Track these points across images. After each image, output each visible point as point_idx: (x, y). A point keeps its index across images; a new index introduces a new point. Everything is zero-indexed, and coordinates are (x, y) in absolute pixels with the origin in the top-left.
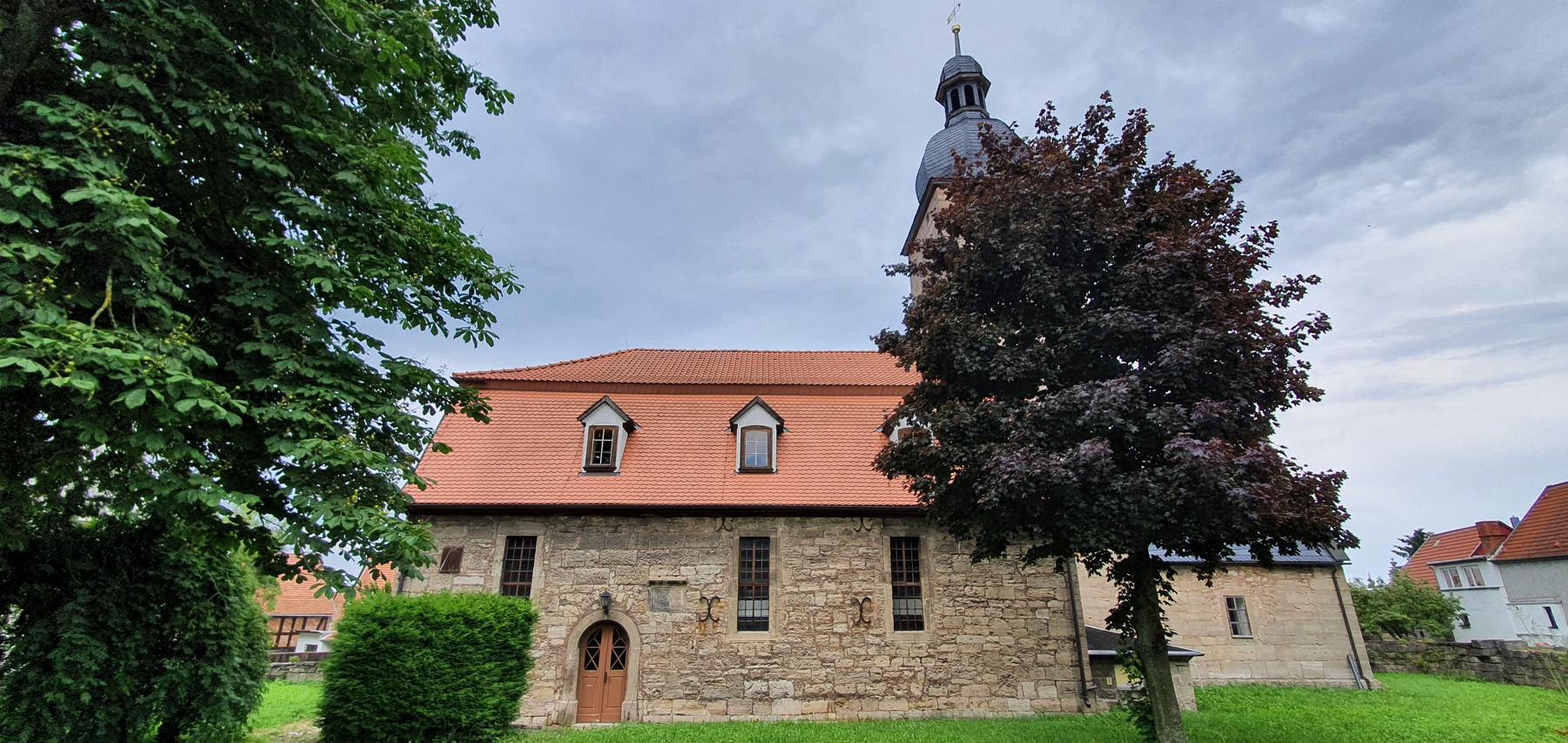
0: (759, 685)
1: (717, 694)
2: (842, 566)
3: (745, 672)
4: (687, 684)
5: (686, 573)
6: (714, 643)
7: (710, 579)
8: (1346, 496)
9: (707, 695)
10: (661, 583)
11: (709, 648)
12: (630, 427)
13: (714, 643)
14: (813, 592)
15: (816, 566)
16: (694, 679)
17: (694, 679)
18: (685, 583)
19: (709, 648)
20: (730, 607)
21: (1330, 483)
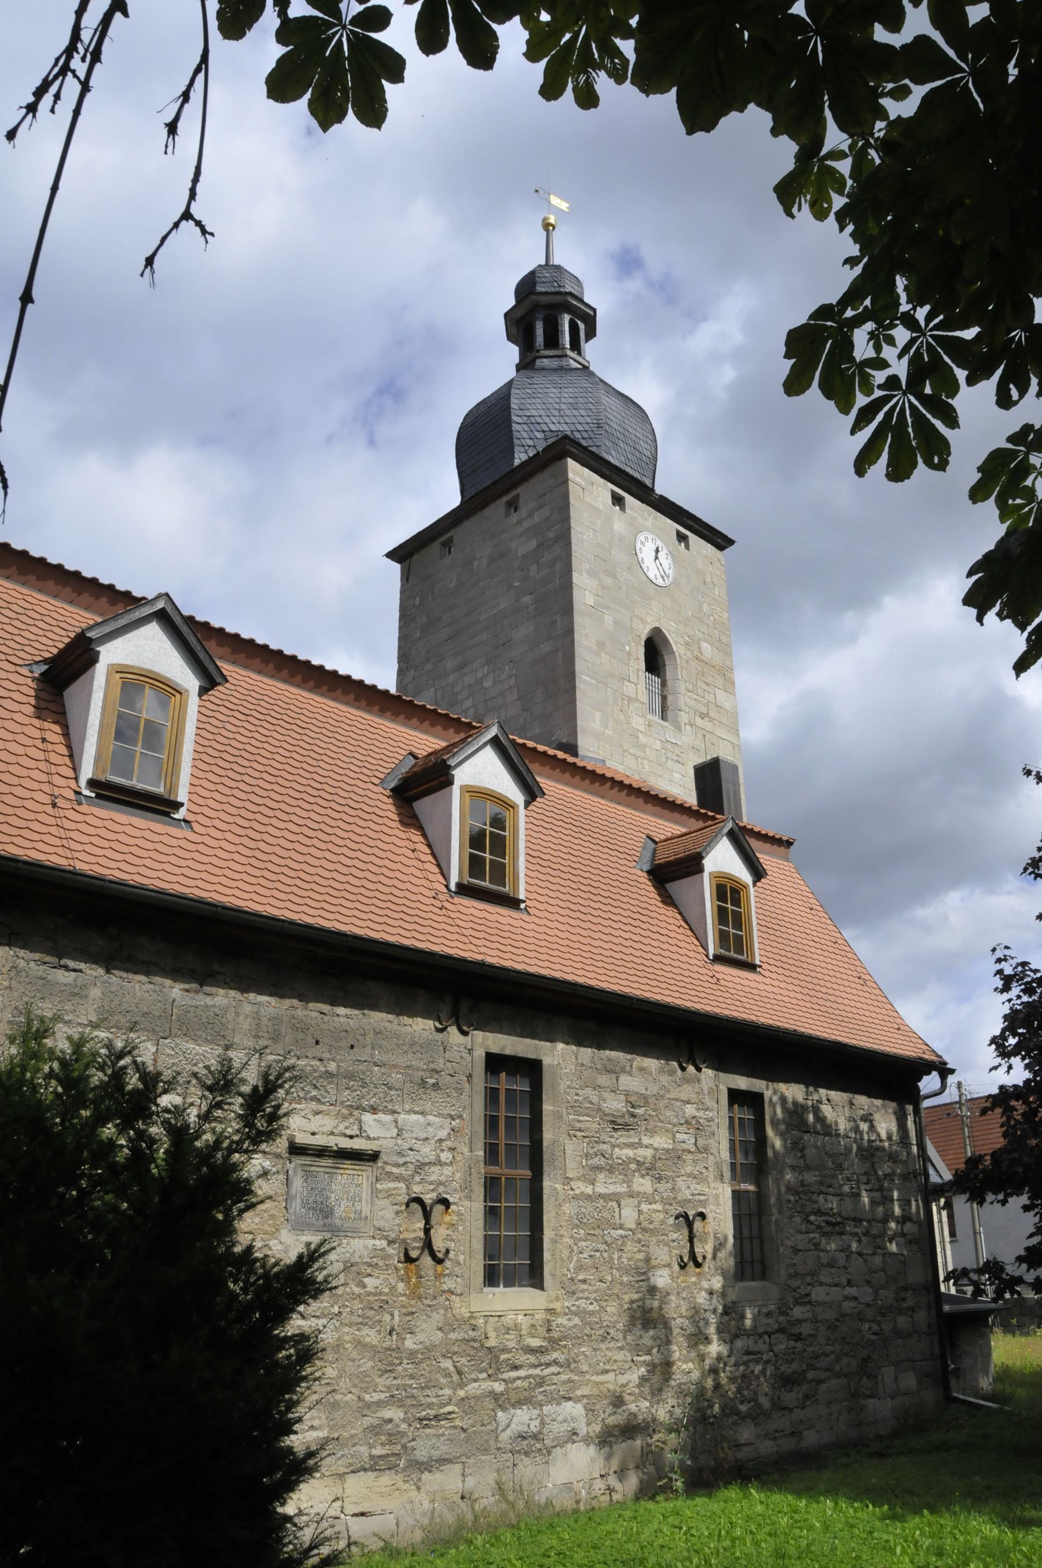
0: (523, 1418)
1: (443, 1449)
2: (661, 1142)
3: (498, 1387)
4: (374, 1430)
5: (377, 1130)
6: (438, 1317)
7: (427, 1152)
8: (376, 130)
9: (422, 1454)
10: (321, 1152)
11: (427, 1332)
12: (1007, 947)
13: (438, 1317)
14: (616, 1198)
15: (622, 1137)
16: (395, 1413)
17: (395, 1413)
18: (374, 1157)
19: (427, 1332)
20: (464, 1230)
21: (647, 96)
